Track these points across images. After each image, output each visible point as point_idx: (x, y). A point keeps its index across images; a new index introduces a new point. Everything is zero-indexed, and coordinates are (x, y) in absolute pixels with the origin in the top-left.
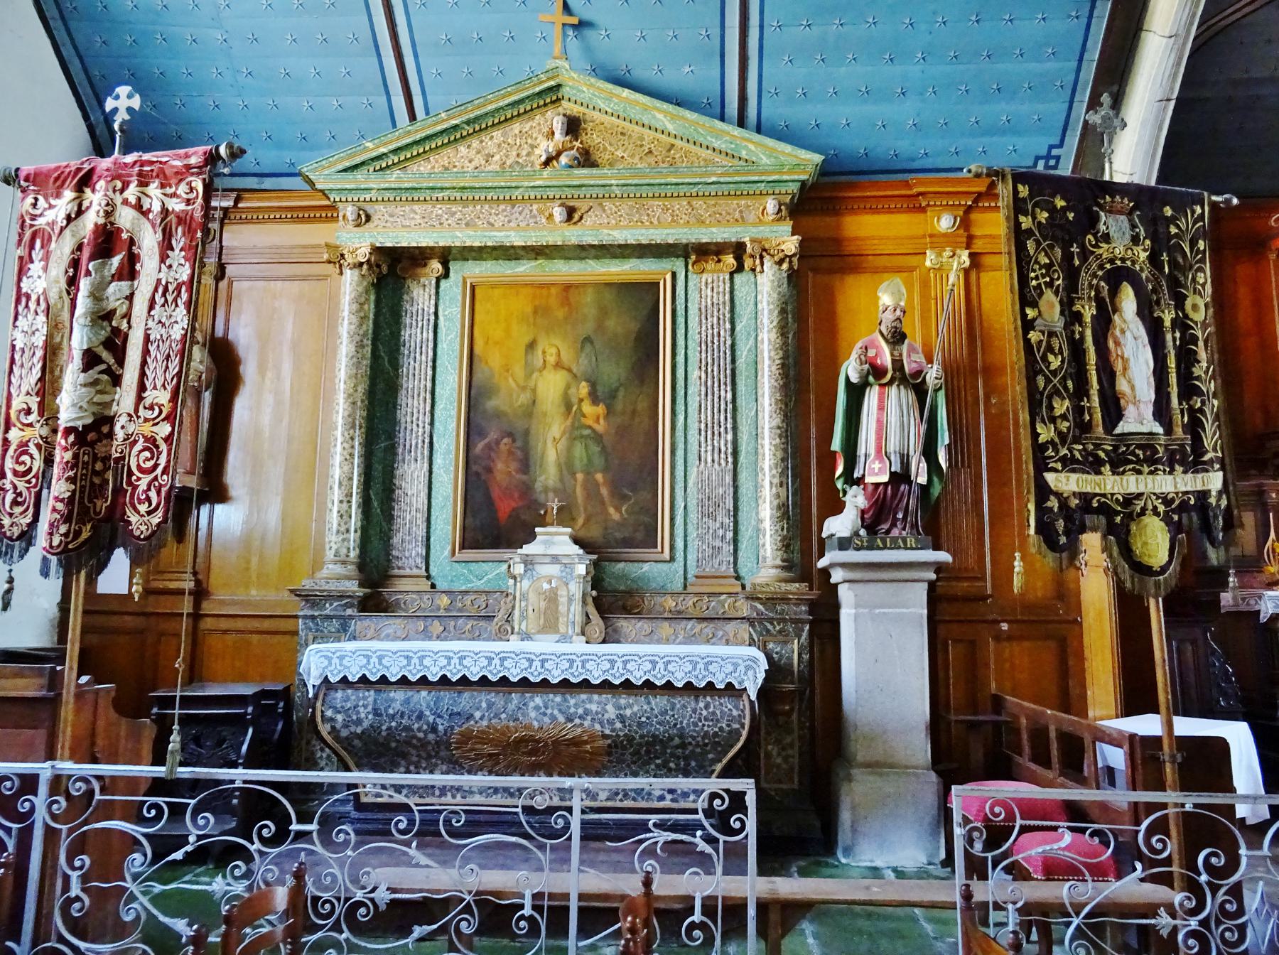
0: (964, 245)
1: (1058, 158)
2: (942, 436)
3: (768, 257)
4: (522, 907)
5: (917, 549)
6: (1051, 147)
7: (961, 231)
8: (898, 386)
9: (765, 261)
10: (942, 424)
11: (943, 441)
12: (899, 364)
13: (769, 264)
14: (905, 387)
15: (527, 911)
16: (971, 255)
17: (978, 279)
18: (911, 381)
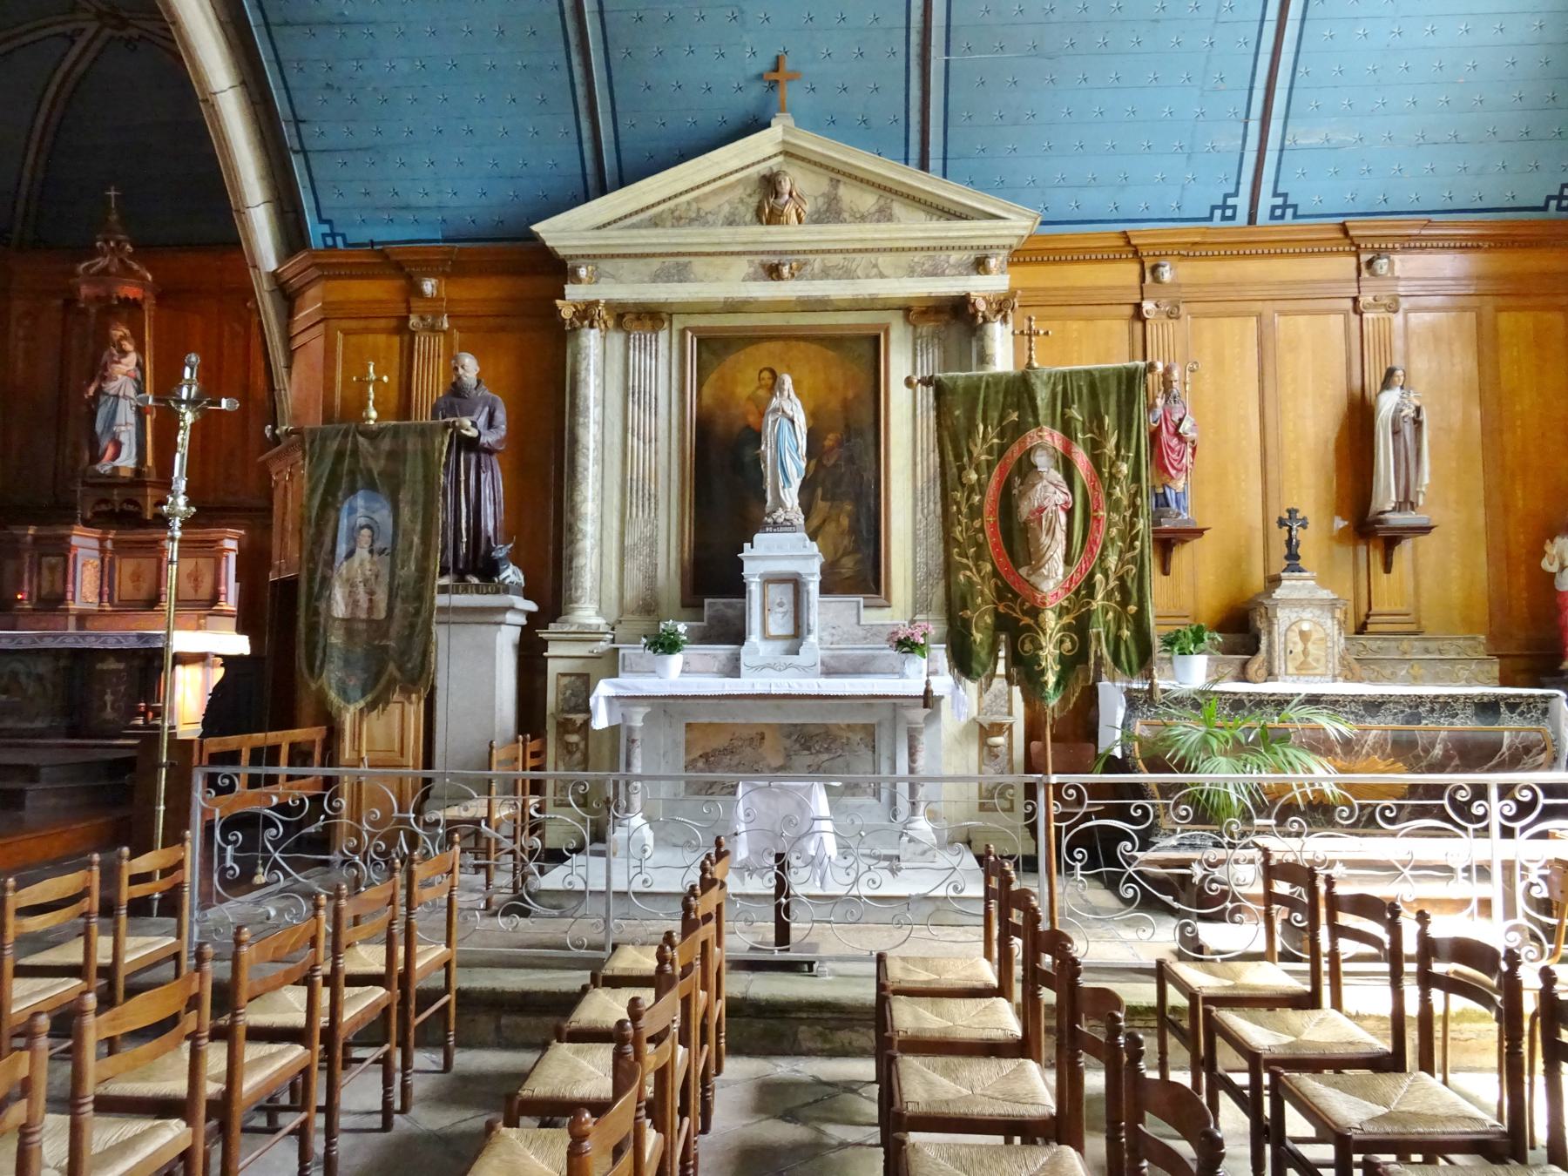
1: (1234, 207)
4: (1083, 868)
6: (1226, 196)
15: (1079, 865)
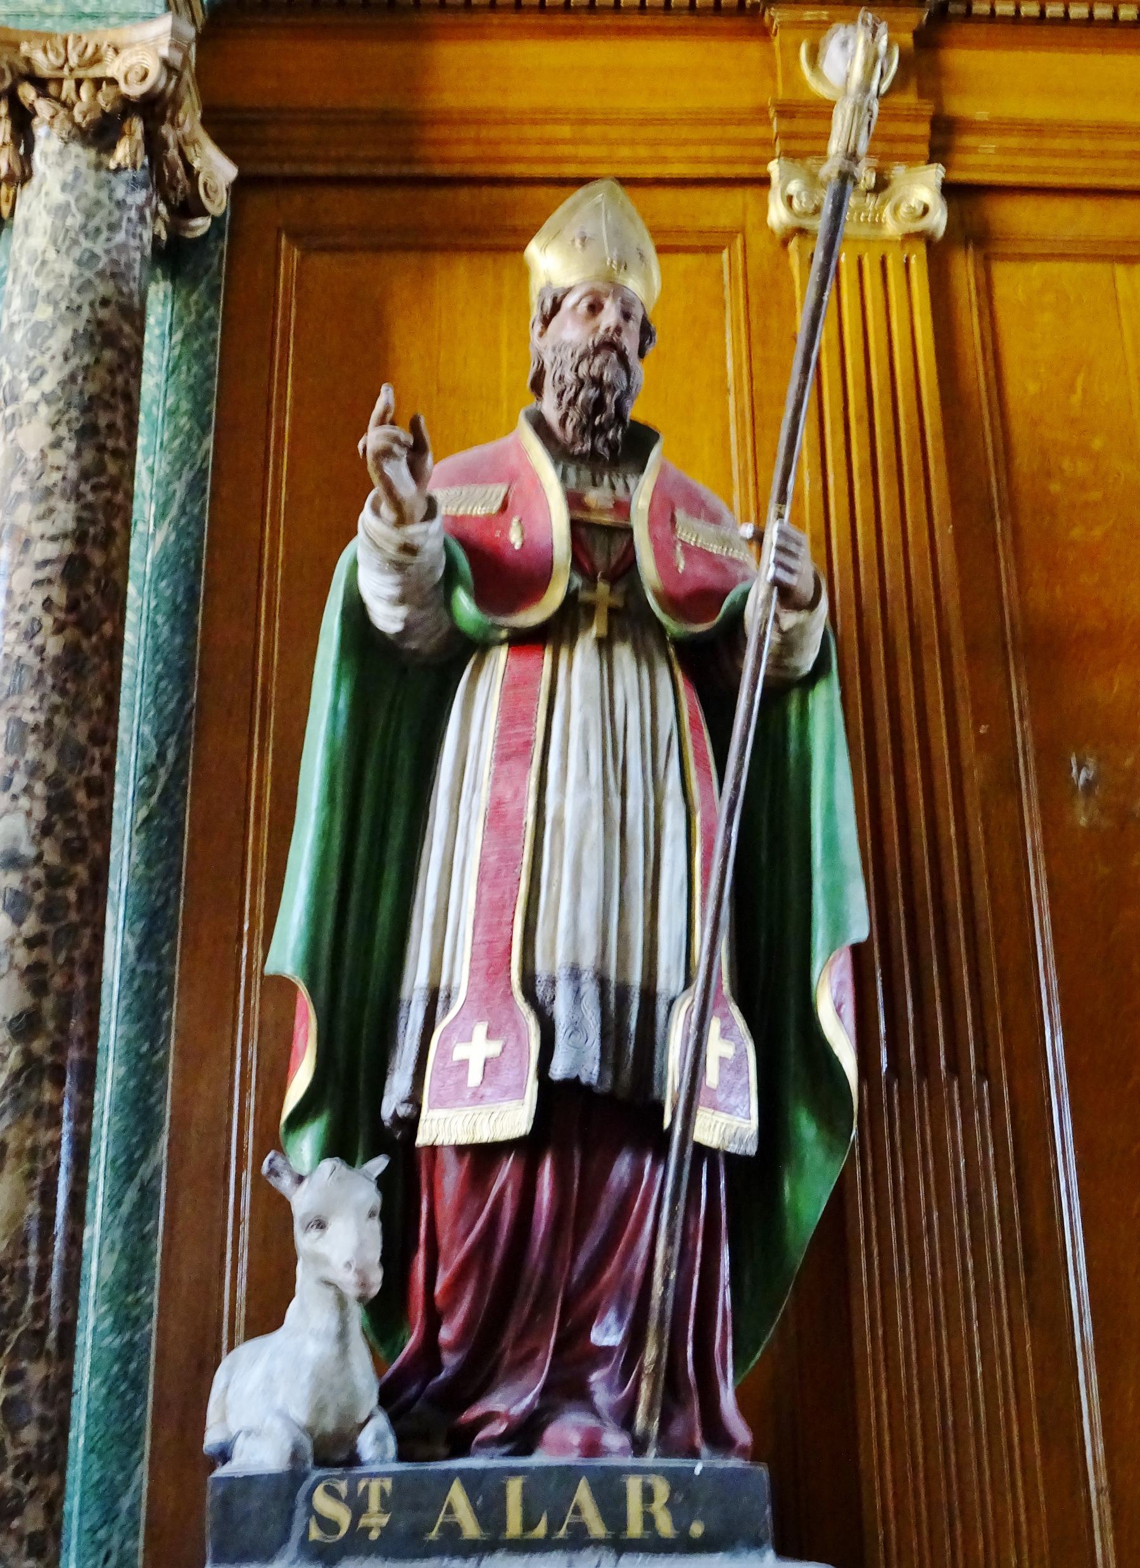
0: (924, 149)
2: (836, 892)
3: (43, 108)
5: (685, 1545)
7: (909, 99)
8: (604, 645)
9: (40, 130)
10: (830, 808)
11: (837, 926)
12: (619, 545)
13: (56, 144)
14: (641, 654)
16: (950, 190)
17: (986, 289)
18: (673, 627)
